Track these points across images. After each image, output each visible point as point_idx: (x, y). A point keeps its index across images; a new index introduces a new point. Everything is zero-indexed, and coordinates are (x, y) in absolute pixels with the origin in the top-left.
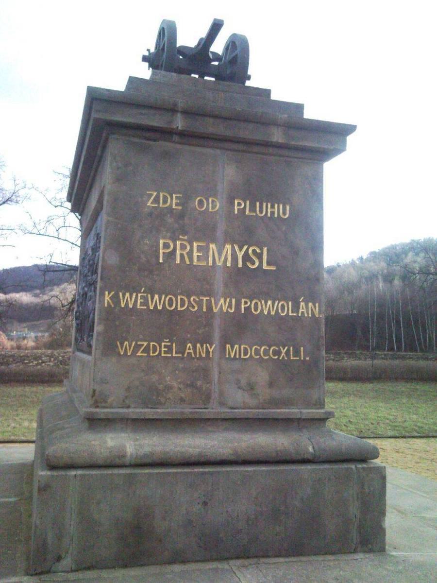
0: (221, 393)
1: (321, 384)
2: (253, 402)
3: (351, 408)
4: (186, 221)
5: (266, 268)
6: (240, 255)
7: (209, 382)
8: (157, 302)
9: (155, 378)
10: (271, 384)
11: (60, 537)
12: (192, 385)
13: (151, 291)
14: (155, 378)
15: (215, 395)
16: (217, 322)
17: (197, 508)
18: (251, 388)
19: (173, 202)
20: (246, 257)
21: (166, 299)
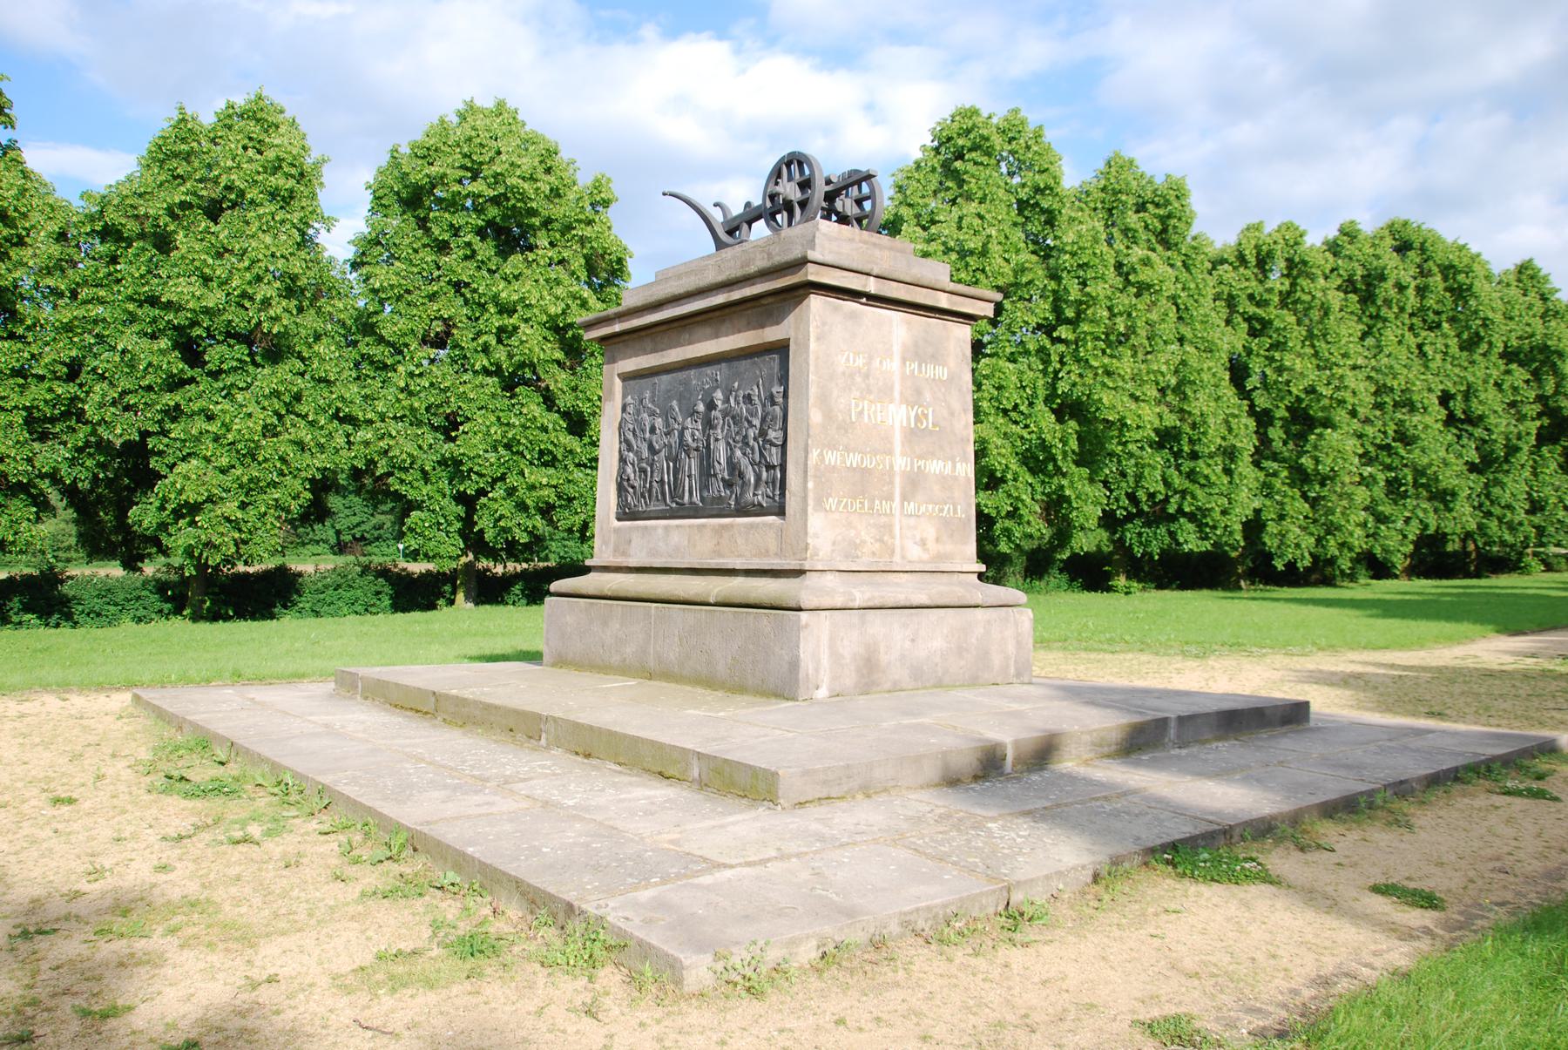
0: (902, 548)
1: (1180, 870)
2: (925, 557)
3: (351, 910)
4: (872, 381)
5: (1083, 771)
6: (913, 414)
7: (893, 537)
8: (854, 460)
9: (853, 533)
10: (937, 540)
11: (817, 670)
12: (881, 541)
13: (848, 449)
14: (853, 533)
15: (898, 550)
16: (897, 480)
17: (908, 644)
18: (923, 543)
19: (860, 362)
20: (917, 417)
21: (858, 457)
